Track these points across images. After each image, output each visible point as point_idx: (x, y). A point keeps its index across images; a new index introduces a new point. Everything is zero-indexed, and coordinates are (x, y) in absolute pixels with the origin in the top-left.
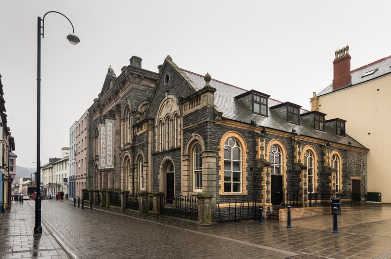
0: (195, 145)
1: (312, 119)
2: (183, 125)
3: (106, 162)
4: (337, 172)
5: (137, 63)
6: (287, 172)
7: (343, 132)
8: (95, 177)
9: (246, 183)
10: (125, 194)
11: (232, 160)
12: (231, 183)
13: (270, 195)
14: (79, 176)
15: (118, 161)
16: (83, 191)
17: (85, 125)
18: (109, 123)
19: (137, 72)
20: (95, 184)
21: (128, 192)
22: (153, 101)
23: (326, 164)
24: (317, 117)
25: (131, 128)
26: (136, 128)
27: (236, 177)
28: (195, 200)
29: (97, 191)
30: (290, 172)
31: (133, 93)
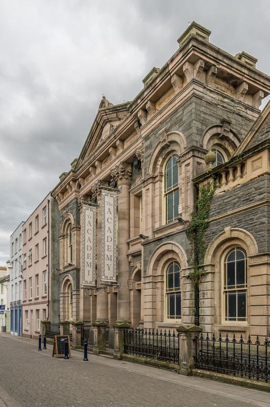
8: (64, 300)
16: (43, 323)
17: (45, 218)
20: (64, 312)
29: (66, 324)
31: (193, 105)
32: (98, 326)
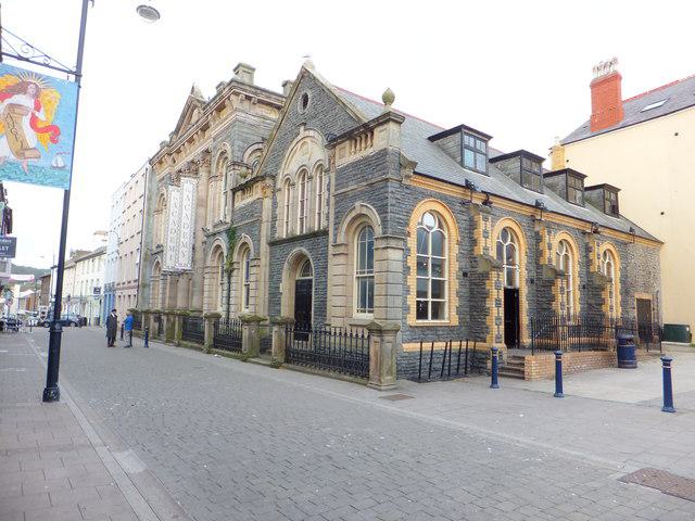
0: (364, 228)
1: (563, 183)
2: (336, 186)
3: (177, 257)
4: (567, 278)
5: (246, 75)
6: (527, 281)
7: (615, 211)
9: (456, 302)
10: (213, 320)
11: (430, 255)
12: (427, 302)
13: (502, 327)
14: (129, 282)
15: (199, 255)
18: (188, 184)
19: (245, 90)
21: (218, 316)
22: (276, 143)
23: (594, 268)
24: (572, 181)
25: (230, 193)
26: (239, 193)
27: (438, 288)
28: (363, 336)
30: (532, 281)
32: (167, 314)
